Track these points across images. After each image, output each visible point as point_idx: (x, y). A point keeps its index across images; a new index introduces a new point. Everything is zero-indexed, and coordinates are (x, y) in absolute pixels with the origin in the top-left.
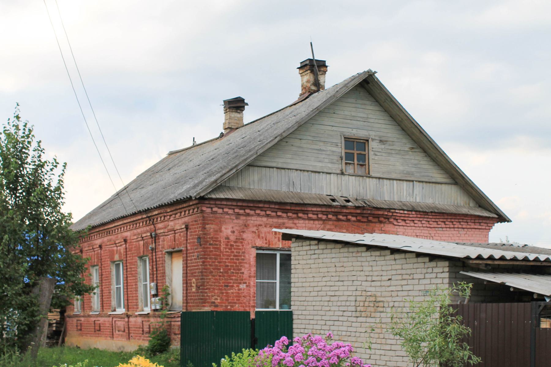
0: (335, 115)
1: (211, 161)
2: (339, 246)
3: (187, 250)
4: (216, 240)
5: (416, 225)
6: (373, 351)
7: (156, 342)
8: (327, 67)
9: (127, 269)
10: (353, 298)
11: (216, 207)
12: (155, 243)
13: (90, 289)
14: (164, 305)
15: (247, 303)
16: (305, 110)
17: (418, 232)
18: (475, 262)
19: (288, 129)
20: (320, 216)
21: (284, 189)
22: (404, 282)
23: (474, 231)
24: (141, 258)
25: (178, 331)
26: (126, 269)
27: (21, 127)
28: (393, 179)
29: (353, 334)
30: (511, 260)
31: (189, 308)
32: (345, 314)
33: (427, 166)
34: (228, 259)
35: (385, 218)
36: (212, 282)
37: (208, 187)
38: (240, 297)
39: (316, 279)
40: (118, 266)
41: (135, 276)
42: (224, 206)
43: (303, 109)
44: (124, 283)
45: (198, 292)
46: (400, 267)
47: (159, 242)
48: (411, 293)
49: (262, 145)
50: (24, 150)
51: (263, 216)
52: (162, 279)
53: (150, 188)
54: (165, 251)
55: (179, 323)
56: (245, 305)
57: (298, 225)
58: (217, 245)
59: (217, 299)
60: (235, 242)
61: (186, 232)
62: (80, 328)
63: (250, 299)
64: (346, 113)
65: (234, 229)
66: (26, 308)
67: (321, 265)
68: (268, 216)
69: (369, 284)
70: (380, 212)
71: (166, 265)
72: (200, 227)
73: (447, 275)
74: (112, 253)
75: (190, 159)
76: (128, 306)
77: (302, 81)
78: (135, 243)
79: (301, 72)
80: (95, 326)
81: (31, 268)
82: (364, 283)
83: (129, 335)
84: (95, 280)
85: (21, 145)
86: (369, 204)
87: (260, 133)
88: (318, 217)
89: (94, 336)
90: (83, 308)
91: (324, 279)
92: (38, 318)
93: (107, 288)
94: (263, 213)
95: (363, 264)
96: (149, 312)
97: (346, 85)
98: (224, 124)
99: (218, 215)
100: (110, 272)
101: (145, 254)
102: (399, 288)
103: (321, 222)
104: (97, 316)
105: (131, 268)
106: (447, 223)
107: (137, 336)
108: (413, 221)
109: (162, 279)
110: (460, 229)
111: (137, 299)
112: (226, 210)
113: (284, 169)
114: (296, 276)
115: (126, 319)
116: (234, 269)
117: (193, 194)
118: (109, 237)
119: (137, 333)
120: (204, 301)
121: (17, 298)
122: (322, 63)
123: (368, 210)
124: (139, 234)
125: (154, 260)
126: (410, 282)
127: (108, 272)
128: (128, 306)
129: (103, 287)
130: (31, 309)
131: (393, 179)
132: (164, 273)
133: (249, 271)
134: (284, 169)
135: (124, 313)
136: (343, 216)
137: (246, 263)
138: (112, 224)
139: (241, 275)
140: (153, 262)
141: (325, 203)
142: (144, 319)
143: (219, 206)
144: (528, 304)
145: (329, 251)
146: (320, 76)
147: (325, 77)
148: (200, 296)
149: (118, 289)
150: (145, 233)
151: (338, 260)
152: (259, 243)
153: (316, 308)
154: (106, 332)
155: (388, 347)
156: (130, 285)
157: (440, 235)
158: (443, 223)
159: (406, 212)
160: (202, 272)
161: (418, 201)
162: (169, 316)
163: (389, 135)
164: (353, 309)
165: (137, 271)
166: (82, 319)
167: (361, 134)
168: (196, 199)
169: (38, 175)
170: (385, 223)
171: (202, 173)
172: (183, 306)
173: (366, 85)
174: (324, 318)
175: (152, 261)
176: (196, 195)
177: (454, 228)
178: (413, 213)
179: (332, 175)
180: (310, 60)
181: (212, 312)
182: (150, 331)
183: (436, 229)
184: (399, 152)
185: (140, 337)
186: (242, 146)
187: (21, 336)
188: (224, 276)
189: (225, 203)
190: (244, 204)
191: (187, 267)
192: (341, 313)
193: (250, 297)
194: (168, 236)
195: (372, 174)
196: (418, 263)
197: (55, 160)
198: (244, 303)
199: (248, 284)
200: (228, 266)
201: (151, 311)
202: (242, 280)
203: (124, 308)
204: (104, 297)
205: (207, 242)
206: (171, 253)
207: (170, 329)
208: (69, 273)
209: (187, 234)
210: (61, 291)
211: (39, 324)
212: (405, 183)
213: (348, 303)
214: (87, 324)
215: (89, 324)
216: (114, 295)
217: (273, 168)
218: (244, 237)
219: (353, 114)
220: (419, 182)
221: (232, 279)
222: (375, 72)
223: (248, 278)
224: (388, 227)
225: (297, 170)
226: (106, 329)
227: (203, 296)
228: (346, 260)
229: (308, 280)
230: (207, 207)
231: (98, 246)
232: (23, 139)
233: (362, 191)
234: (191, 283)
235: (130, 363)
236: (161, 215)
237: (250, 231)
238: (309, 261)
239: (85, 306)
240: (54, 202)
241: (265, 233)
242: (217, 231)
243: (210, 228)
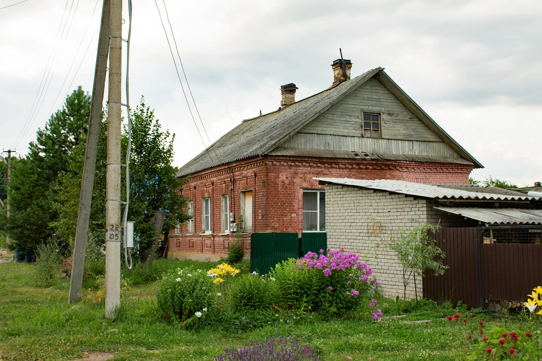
1: (272, 129)
2: (356, 189)
3: (255, 190)
4: (276, 183)
5: (415, 171)
6: (379, 260)
8: (351, 64)
10: (366, 224)
12: (233, 185)
13: (188, 218)
14: (239, 229)
15: (297, 227)
16: (335, 94)
17: (417, 176)
18: (442, 200)
19: (324, 108)
20: (347, 166)
21: (322, 148)
22: (399, 214)
24: (223, 195)
25: (249, 247)
27: (145, 111)
28: (398, 140)
29: (366, 248)
30: (467, 199)
31: (256, 231)
32: (361, 234)
35: (393, 167)
37: (270, 148)
38: (292, 222)
39: (342, 211)
40: (207, 201)
41: (219, 208)
42: (281, 161)
43: (334, 94)
44: (211, 213)
45: (263, 220)
46: (395, 203)
48: (403, 221)
49: (307, 119)
50: (147, 126)
52: (238, 211)
53: (230, 146)
55: (250, 241)
57: (332, 172)
58: (276, 187)
59: (276, 224)
60: (289, 185)
62: (179, 245)
65: (288, 176)
66: (146, 231)
67: (345, 202)
68: (311, 166)
69: (376, 214)
70: (389, 163)
71: (241, 200)
72: (264, 175)
73: (425, 209)
74: (203, 192)
75: (258, 126)
76: (214, 229)
77: (335, 73)
81: (150, 205)
82: (373, 214)
84: (190, 212)
85: (145, 123)
86: (381, 157)
87: (306, 109)
90: (181, 231)
91: (347, 211)
92: (154, 239)
94: (308, 165)
95: (372, 201)
97: (363, 78)
98: (282, 102)
99: (277, 167)
101: (226, 193)
102: (395, 217)
103: (348, 170)
105: (216, 203)
106: (438, 169)
107: (219, 251)
108: (414, 168)
109: (238, 211)
110: (447, 174)
111: (220, 225)
112: (282, 163)
113: (322, 134)
114: (329, 209)
115: (212, 239)
116: (288, 204)
117: (260, 152)
118: (201, 181)
120: (267, 226)
121: (140, 225)
122: (348, 62)
123: (381, 161)
124: (222, 179)
125: (233, 197)
126: (402, 213)
128: (214, 229)
130: (149, 232)
131: (398, 140)
134: (322, 134)
136: (363, 166)
137: (296, 199)
141: (351, 157)
142: (224, 239)
143: (278, 160)
144: (475, 228)
145: (350, 192)
146: (346, 70)
148: (264, 222)
149: (207, 217)
150: (226, 178)
151: (355, 198)
152: (305, 185)
153: (342, 231)
155: (389, 257)
158: (435, 170)
159: (407, 162)
160: (265, 206)
161: (416, 154)
163: (395, 110)
164: (366, 231)
166: (181, 239)
167: (376, 109)
168: (262, 156)
169: (156, 143)
170: (393, 170)
171: (266, 137)
173: (378, 77)
174: (347, 237)
175: (231, 198)
176: (262, 154)
177: (443, 172)
178: (413, 163)
179: (355, 138)
181: (273, 233)
182: (229, 247)
183: (430, 174)
184: (402, 121)
186: (293, 118)
187: (142, 251)
188: (280, 208)
189: (281, 158)
191: (255, 202)
192: (358, 234)
195: (383, 136)
196: (407, 201)
197: (168, 132)
200: (283, 201)
203: (211, 231)
205: (269, 185)
206: (244, 193)
207: (243, 245)
208: (175, 208)
210: (169, 220)
211: (154, 243)
212: (407, 142)
213: (363, 228)
217: (314, 134)
219: (369, 96)
220: (417, 141)
221: (287, 210)
222: (384, 69)
225: (331, 135)
227: (266, 222)
228: (361, 198)
229: (336, 212)
232: (147, 119)
233: (376, 148)
234: (258, 213)
235: (218, 268)
236: (238, 166)
238: (337, 199)
240: (166, 160)
242: (276, 177)
243: (271, 175)
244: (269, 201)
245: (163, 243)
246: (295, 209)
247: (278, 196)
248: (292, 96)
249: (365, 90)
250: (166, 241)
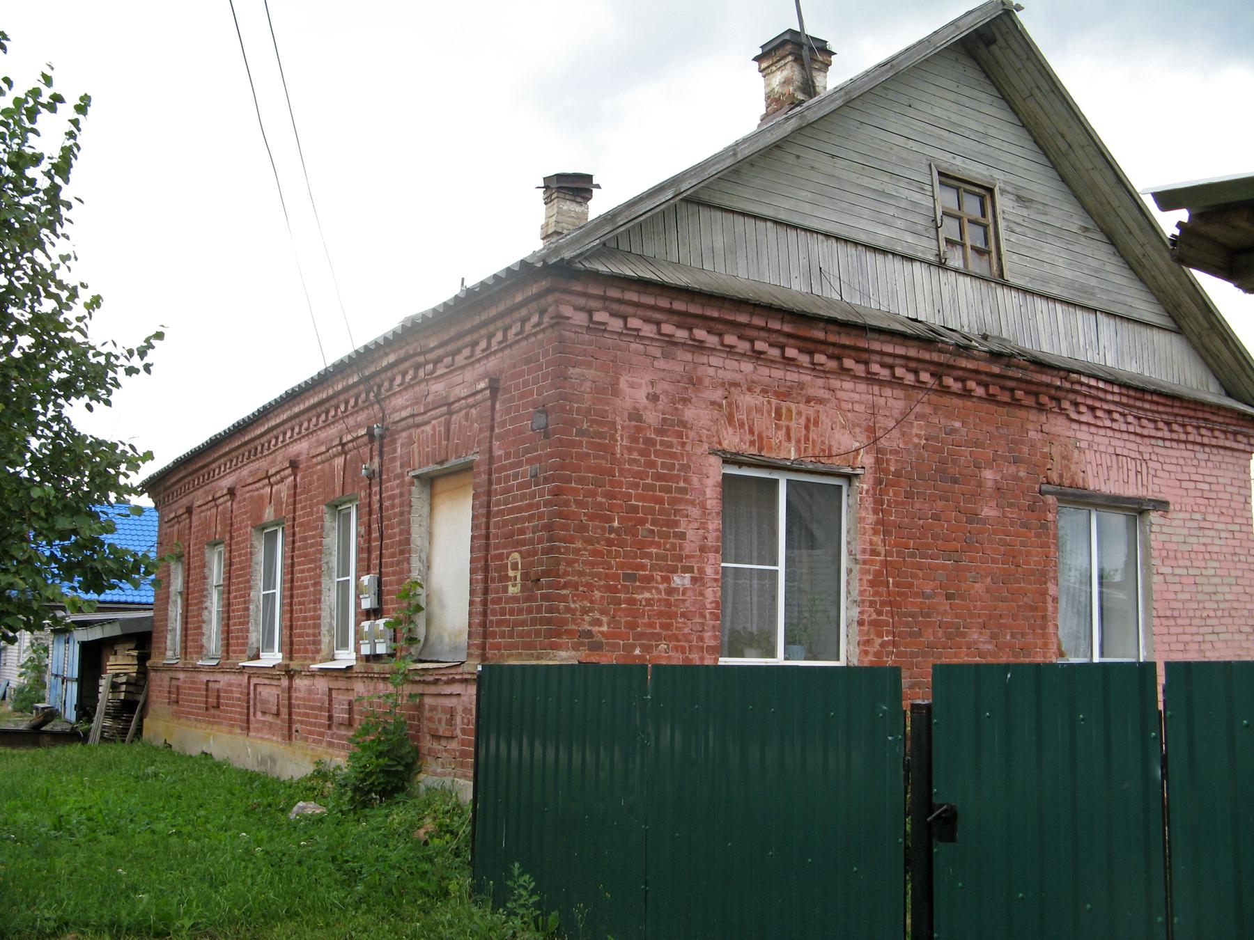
0: (911, 112)
3: (491, 460)
7: (372, 763)
9: (294, 542)
11: (605, 309)
12: (381, 455)
21: (798, 286)
23: (1223, 456)
24: (334, 507)
26: (291, 545)
31: (490, 653)
33: (1120, 277)
34: (636, 486)
36: (585, 563)
38: (672, 616)
42: (631, 310)
44: (283, 582)
45: (527, 599)
47: (395, 451)
51: (744, 355)
52: (399, 563)
54: (412, 474)
56: (687, 645)
57: (839, 394)
58: (601, 435)
59: (598, 622)
60: (660, 432)
61: (489, 403)
63: (702, 624)
64: (938, 112)
68: (757, 356)
71: (414, 517)
72: (545, 378)
74: (259, 503)
76: (291, 643)
77: (767, 85)
78: (319, 467)
79: (764, 65)
80: (207, 696)
83: (290, 728)
88: (893, 375)
89: (204, 721)
93: (241, 596)
94: (744, 346)
96: (354, 663)
99: (609, 340)
100: (251, 554)
103: (899, 393)
104: (212, 670)
105: (304, 539)
107: (311, 733)
109: (399, 563)
111: (317, 626)
115: (285, 682)
116: (654, 523)
119: (311, 724)
120: (555, 631)
125: (376, 506)
127: (246, 554)
128: (291, 643)
129: (232, 595)
132: (408, 541)
133: (701, 532)
135: (279, 665)
137: (692, 503)
138: (263, 424)
139: (677, 541)
140: (370, 513)
142: (333, 685)
143: (616, 307)
146: (815, 74)
147: (826, 77)
149: (269, 599)
152: (732, 440)
154: (231, 712)
156: (300, 588)
157: (1161, 459)
160: (549, 527)
162: (417, 678)
163: (1035, 187)
165: (321, 544)
166: (181, 676)
172: (469, 646)
173: (983, 51)
175: (367, 512)
177: (1186, 442)
179: (917, 265)
180: (790, 31)
184: (1059, 233)
185: (322, 734)
188: (622, 544)
189: (633, 296)
190: (695, 309)
191: (488, 515)
193: (705, 617)
194: (423, 428)
198: (686, 637)
199: (696, 574)
200: (635, 509)
201: (357, 659)
202: (680, 558)
204: (231, 622)
205: (573, 423)
206: (429, 482)
209: (493, 408)
214: (190, 688)
215: (195, 689)
216: (258, 616)
217: (765, 219)
218: (686, 418)
219: (955, 118)
221: (649, 556)
222: (1019, 8)
223: (698, 553)
224: (1055, 425)
226: (233, 706)
230: (577, 309)
231: (225, 491)
233: (988, 318)
236: (407, 364)
237: (704, 399)
239: (189, 644)
241: (749, 410)
244: (567, 503)
245: (131, 689)
246: (686, 552)
247: (612, 483)
248: (578, 209)
249: (933, 90)
250: (142, 683)
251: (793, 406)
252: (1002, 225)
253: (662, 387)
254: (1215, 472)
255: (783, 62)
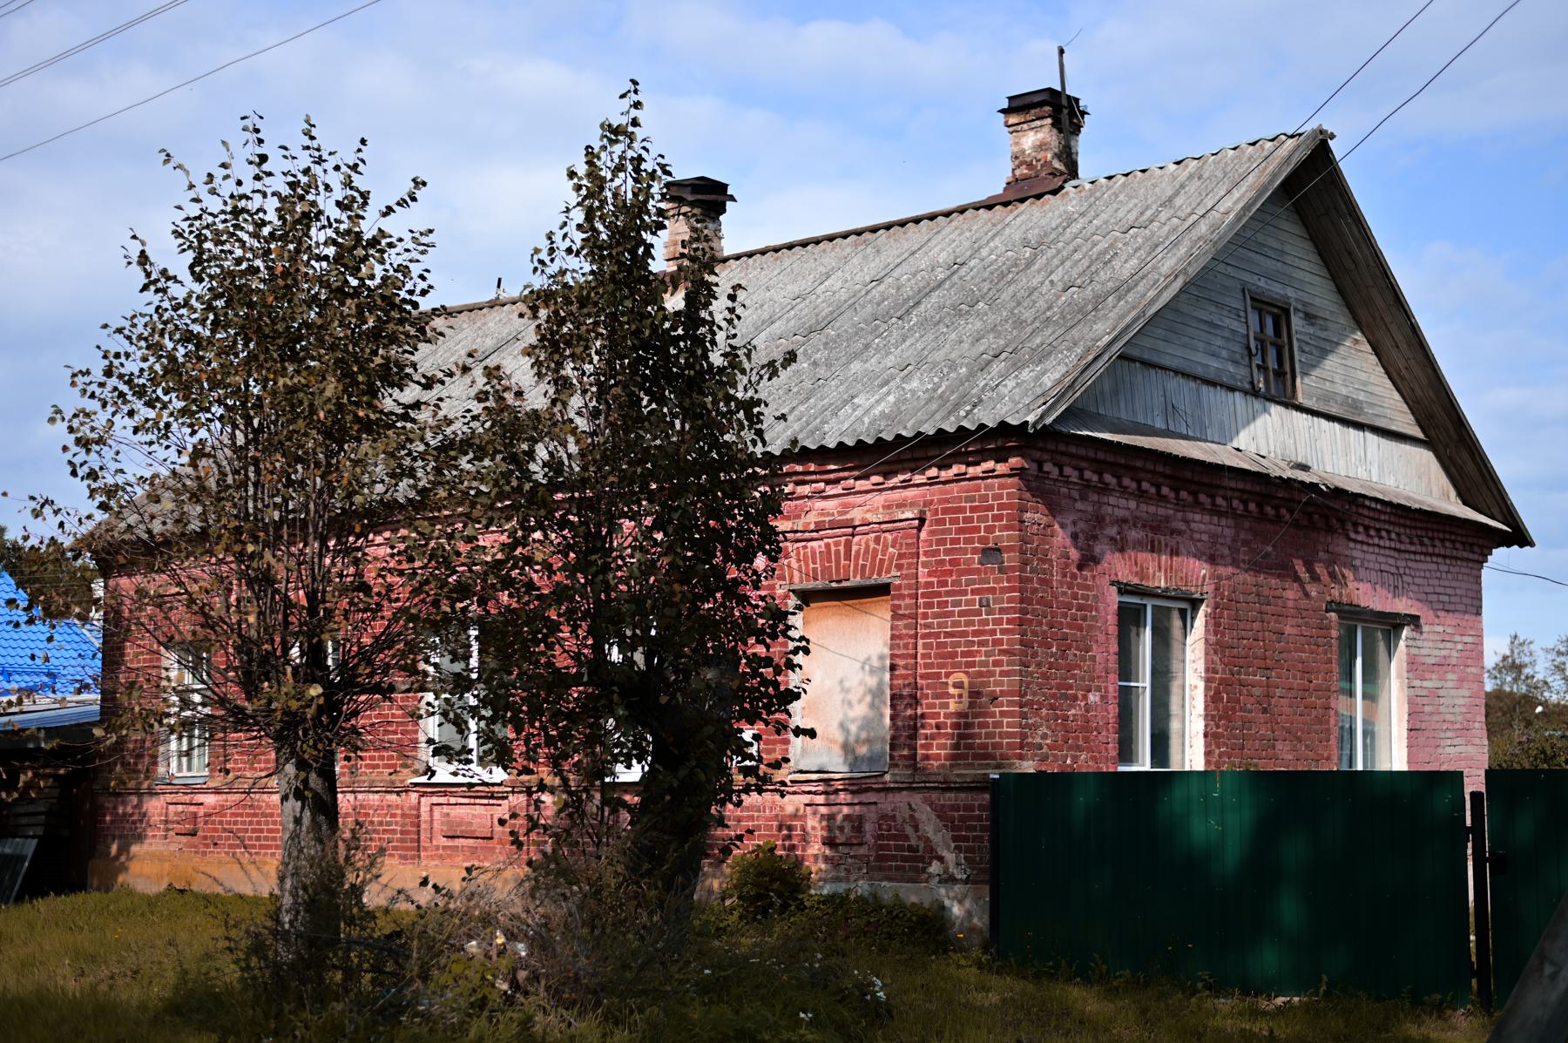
57: (1193, 525)
68: (1141, 495)
163: (1317, 301)
177: (1431, 555)
180: (1050, 90)
251: (1162, 538)
252: (1296, 345)
253: (1081, 525)
254: (1454, 584)
255: (1038, 123)
